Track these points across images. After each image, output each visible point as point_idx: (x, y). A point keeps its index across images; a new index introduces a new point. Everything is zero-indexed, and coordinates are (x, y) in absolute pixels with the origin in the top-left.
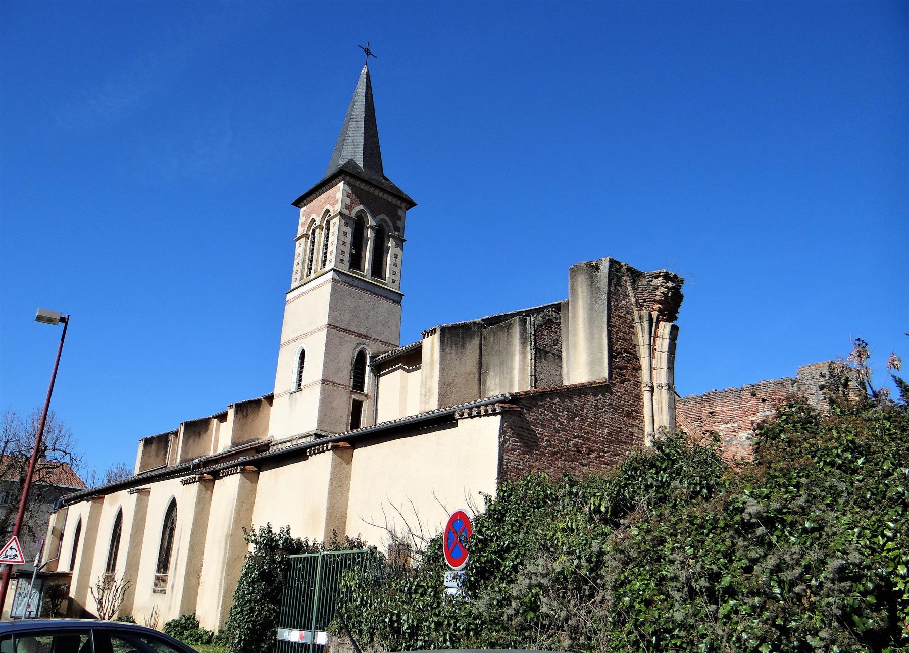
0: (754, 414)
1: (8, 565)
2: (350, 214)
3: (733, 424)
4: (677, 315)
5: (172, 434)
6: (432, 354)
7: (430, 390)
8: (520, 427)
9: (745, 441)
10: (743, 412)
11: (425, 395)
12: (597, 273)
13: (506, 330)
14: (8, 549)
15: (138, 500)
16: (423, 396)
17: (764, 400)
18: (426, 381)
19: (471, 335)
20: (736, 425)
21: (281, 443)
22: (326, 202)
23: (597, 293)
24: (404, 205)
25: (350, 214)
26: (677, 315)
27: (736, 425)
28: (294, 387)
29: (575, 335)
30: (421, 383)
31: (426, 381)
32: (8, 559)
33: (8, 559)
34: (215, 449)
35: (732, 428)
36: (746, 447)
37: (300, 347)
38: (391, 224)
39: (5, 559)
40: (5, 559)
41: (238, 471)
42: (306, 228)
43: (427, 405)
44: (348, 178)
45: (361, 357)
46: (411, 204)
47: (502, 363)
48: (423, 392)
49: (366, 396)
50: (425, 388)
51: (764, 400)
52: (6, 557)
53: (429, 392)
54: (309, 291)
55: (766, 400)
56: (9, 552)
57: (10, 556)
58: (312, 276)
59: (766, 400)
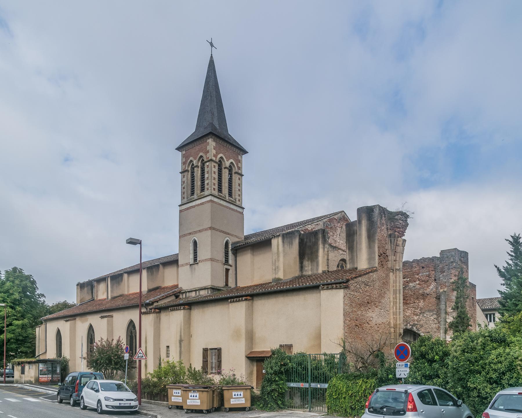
0: (418, 274)
1: (139, 360)
2: (216, 160)
3: (407, 279)
4: (405, 233)
5: (95, 281)
6: (278, 249)
7: (278, 267)
8: (349, 294)
9: (412, 288)
10: (413, 273)
11: (275, 270)
12: (372, 213)
13: (314, 236)
14: (139, 353)
15: (108, 321)
16: (274, 270)
17: (423, 267)
18: (275, 262)
19: (295, 238)
20: (408, 279)
21: (189, 292)
22: (200, 151)
23: (372, 224)
24: (241, 153)
25: (216, 160)
26: (405, 233)
27: (408, 279)
28: (192, 262)
29: (361, 244)
30: (272, 263)
31: (275, 262)
32: (139, 358)
33: (139, 358)
34: (128, 291)
35: (406, 281)
36: (413, 290)
37: (193, 238)
38: (236, 166)
39: (138, 358)
40: (138, 358)
41: (182, 308)
42: (187, 166)
43: (276, 275)
44: (213, 137)
45: (227, 243)
46: (245, 152)
47: (312, 253)
48: (274, 268)
49: (231, 266)
50: (275, 266)
51: (423, 267)
52: (139, 357)
53: (278, 269)
54: (196, 205)
55: (424, 268)
56: (139, 355)
57: (140, 357)
58: (195, 196)
59: (424, 268)
